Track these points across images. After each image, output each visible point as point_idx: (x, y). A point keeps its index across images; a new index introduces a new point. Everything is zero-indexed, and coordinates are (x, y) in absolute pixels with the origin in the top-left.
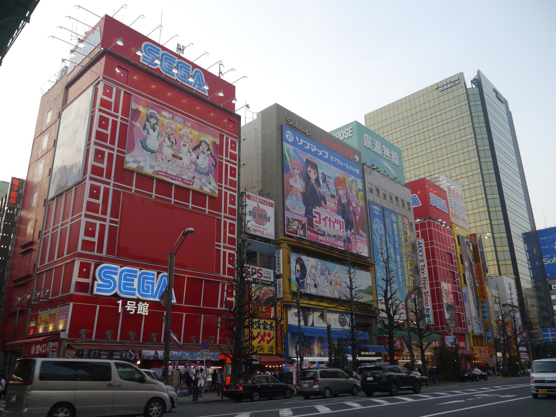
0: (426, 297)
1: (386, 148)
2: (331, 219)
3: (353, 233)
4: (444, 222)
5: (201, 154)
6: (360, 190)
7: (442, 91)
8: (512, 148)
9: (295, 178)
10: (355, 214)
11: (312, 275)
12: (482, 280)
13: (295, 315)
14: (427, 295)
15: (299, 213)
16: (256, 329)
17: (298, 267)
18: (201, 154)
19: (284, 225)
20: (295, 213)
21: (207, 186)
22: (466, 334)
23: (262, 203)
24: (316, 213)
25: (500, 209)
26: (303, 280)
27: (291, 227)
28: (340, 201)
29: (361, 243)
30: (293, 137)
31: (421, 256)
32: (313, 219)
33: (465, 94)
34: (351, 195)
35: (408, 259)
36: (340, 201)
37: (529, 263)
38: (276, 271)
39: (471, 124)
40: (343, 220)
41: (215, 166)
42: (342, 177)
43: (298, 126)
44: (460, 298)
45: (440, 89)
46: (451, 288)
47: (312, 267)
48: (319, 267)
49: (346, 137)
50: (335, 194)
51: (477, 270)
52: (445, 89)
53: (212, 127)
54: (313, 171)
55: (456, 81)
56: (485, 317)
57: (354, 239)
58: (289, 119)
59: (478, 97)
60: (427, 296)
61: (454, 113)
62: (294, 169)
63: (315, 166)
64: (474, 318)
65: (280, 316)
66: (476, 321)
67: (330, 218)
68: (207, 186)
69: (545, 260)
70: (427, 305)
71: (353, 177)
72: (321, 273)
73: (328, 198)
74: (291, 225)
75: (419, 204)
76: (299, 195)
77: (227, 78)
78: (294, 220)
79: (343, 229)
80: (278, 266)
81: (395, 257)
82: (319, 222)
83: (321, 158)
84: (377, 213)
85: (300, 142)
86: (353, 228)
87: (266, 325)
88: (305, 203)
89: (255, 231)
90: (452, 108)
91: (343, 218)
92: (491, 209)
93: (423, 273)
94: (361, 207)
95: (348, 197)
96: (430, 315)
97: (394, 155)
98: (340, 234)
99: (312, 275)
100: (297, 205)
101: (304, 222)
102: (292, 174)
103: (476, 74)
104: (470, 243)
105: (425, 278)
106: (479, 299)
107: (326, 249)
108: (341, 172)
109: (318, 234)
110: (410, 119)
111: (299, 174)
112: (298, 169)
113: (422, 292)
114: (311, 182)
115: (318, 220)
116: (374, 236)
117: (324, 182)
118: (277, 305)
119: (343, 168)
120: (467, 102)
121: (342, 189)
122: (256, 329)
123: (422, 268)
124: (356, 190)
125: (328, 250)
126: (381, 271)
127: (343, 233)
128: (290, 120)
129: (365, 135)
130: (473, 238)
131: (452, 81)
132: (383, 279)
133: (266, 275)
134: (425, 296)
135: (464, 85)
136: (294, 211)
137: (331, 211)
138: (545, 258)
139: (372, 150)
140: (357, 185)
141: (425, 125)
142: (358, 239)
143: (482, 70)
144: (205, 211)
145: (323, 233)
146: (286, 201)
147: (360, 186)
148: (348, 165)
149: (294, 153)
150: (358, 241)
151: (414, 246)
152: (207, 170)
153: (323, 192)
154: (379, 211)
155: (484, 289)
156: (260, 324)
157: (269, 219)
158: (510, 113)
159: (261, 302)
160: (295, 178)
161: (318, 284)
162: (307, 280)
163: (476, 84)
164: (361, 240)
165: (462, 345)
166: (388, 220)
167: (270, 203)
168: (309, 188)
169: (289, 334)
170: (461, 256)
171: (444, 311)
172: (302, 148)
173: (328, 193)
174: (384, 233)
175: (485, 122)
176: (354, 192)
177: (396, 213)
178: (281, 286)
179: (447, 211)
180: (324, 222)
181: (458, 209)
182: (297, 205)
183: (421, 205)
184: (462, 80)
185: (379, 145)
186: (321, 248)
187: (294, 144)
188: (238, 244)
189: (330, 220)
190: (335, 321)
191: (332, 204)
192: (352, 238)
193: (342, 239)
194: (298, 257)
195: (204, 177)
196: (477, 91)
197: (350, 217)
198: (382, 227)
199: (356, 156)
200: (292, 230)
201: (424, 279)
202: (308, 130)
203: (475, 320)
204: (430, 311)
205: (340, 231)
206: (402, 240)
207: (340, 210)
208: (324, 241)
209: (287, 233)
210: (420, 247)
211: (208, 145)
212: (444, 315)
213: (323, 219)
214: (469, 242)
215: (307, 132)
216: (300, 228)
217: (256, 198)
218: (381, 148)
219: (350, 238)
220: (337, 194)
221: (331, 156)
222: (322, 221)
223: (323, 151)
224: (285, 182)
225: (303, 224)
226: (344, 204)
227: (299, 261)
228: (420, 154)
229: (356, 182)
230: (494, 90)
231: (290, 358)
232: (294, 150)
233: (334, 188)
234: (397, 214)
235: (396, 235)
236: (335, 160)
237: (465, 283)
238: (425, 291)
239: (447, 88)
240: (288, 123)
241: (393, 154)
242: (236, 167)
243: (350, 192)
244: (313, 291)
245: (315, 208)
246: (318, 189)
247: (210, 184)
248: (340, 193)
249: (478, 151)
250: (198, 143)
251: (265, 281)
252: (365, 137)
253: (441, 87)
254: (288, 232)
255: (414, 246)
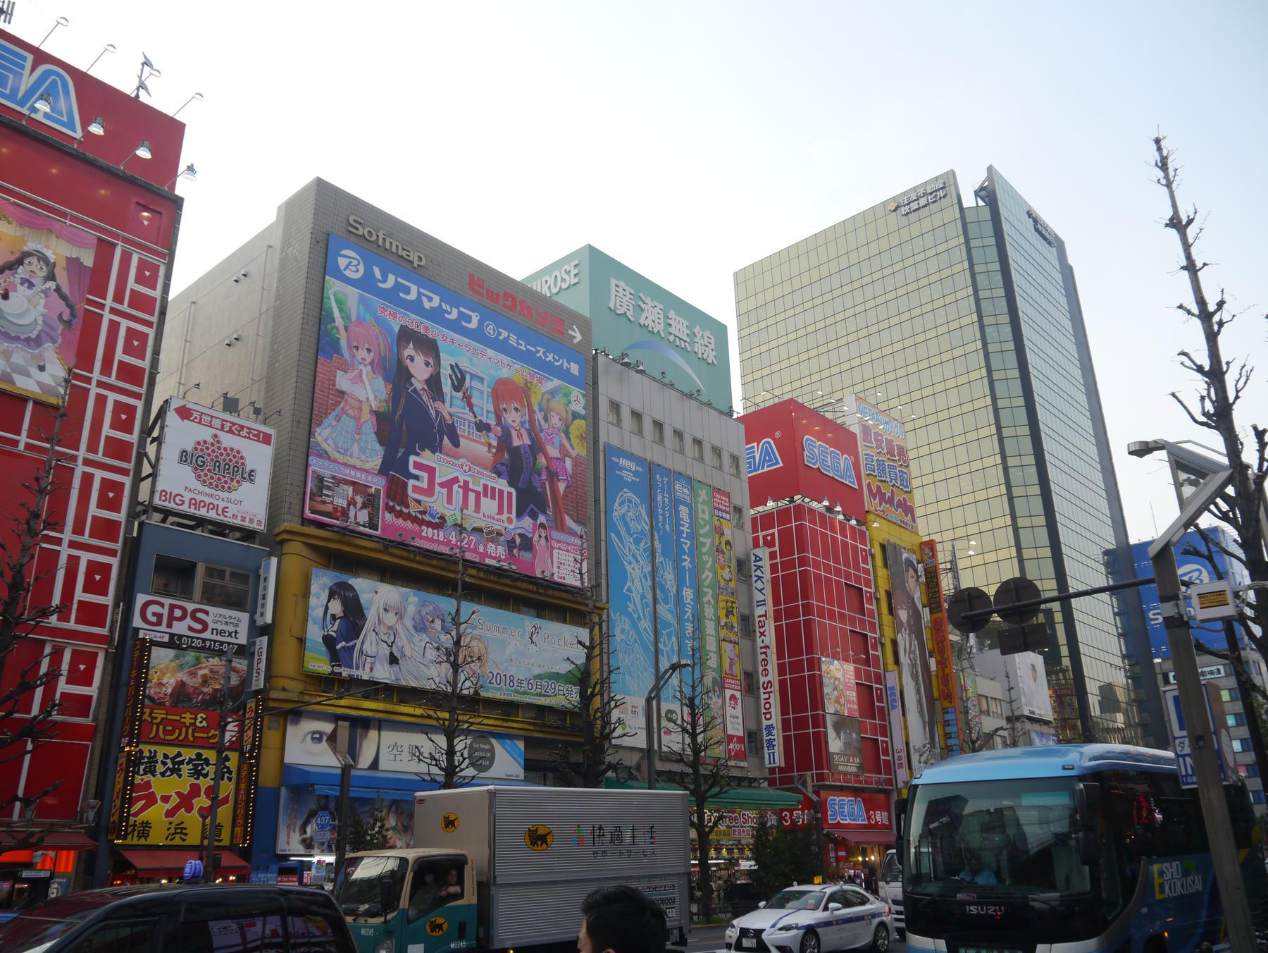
0: (767, 696)
1: (678, 318)
2: (471, 486)
3: (542, 526)
4: (838, 509)
5: (19, 287)
6: (576, 416)
7: (907, 214)
8: (1073, 348)
9: (356, 372)
10: (553, 476)
11: (382, 630)
12: (946, 656)
13: (313, 739)
14: (769, 690)
15: (358, 464)
16: (163, 774)
17: (336, 607)
18: (19, 287)
19: (304, 493)
20: (345, 464)
21: (28, 375)
22: (892, 790)
23: (230, 432)
24: (418, 466)
25: (1037, 490)
26: (351, 644)
27: (328, 500)
28: (505, 440)
29: (568, 551)
30: (361, 268)
31: (760, 591)
32: (407, 483)
33: (959, 222)
34: (545, 426)
35: (721, 597)
36: (505, 440)
37: (1119, 625)
38: (257, 617)
39: (970, 291)
40: (513, 491)
41: (68, 324)
42: (519, 380)
43: (384, 239)
44: (880, 700)
45: (903, 209)
46: (853, 673)
47: (385, 610)
48: (411, 609)
49: (565, 286)
50: (492, 422)
51: (934, 631)
52: (914, 211)
53: (73, 219)
54: (420, 359)
55: (939, 190)
56: (950, 748)
57: (543, 541)
58: (355, 221)
59: (988, 229)
60: (769, 693)
61: (933, 265)
62: (357, 348)
63: (429, 347)
64: (918, 750)
65: (250, 740)
66: (923, 759)
67: (466, 483)
68: (28, 375)
69: (1154, 614)
70: (768, 716)
71: (556, 382)
72: (415, 627)
73: (462, 430)
74: (328, 496)
75: (777, 463)
76: (366, 415)
77: (159, 99)
78: (338, 481)
79: (510, 511)
80: (263, 602)
81: (679, 592)
82: (430, 491)
83: (455, 326)
84: (629, 477)
85: (384, 280)
86: (544, 513)
87: (201, 765)
88: (381, 437)
89: (197, 505)
90: (929, 253)
91: (510, 484)
92: (1016, 492)
93: (762, 634)
94: (577, 462)
95: (533, 431)
96: (774, 743)
97: (702, 336)
98: (497, 526)
99: (382, 630)
100: (356, 444)
101: (373, 490)
102: (349, 361)
103: (984, 175)
104: (919, 563)
105: (767, 647)
106: (938, 704)
107: (435, 562)
108: (516, 366)
109: (422, 523)
110: (836, 282)
111: (372, 363)
112: (369, 350)
113: (758, 682)
114: (412, 385)
115: (424, 485)
116: (612, 535)
117: (457, 388)
118: (248, 710)
119: (526, 358)
120: (962, 239)
121: (516, 409)
122: (163, 774)
123: (760, 621)
124: (564, 414)
125: (443, 564)
126: (627, 627)
127: (506, 524)
128: (361, 224)
129: (613, 281)
130: (927, 550)
131: (929, 191)
132: (580, 642)
133: (220, 627)
134: (764, 693)
135: (955, 201)
136: (341, 459)
137: (472, 464)
138: (1152, 610)
139: (632, 319)
140: (570, 402)
141: (869, 295)
142: (559, 542)
143: (996, 166)
144: (16, 443)
145: (437, 520)
146: (318, 430)
147: (579, 406)
148: (542, 350)
149: (362, 308)
150: (556, 545)
151: (742, 566)
152: (36, 333)
153: (450, 414)
154: (636, 473)
155: (949, 678)
156: (182, 762)
157: (250, 475)
158: (1071, 269)
159: (190, 700)
160: (356, 372)
161: (404, 655)
162: (363, 644)
163: (986, 200)
164: (568, 544)
165: (878, 818)
166: (663, 497)
167: (259, 432)
168: (403, 401)
169: (283, 790)
170: (889, 594)
171: (826, 733)
172: (392, 296)
173: (470, 417)
174: (647, 528)
175: (1004, 287)
176: (555, 420)
177: (689, 480)
178: (264, 657)
179: (853, 483)
180: (445, 491)
181: (888, 480)
182: (356, 444)
183: (781, 465)
184: (953, 188)
185: (657, 310)
186: (417, 558)
187: (366, 284)
188: (126, 539)
189: (466, 487)
190: (395, 752)
191: (477, 446)
192: (536, 538)
193: (502, 539)
194: (338, 580)
195: (22, 349)
196: (986, 215)
197: (536, 484)
198: (644, 513)
199: (574, 330)
200: (329, 508)
201: (764, 650)
202: (417, 254)
203: (921, 755)
204: (774, 732)
205: (499, 517)
206: (704, 550)
207: (502, 464)
208: (438, 542)
209: (308, 513)
210: (759, 567)
211: (51, 266)
212: (827, 743)
213: (442, 485)
214: (915, 563)
215: (413, 257)
216: (359, 505)
217: (212, 417)
218: (661, 317)
219: (532, 539)
220: (499, 422)
221: (488, 325)
222: (437, 488)
223: (462, 309)
224: (321, 381)
225: (371, 495)
226: (518, 448)
227: (339, 591)
228: (856, 362)
229: (567, 395)
230: (1030, 214)
231: (285, 857)
232: (362, 301)
233: (491, 408)
234: (696, 485)
235: (685, 535)
236: (500, 334)
237: (897, 661)
238: (766, 679)
239: (919, 208)
240: (350, 229)
241: (699, 336)
242: (151, 332)
243: (542, 421)
244: (383, 674)
245: (418, 454)
246: (432, 406)
247: (42, 369)
248: (509, 421)
249: (987, 355)
250: (12, 258)
251: (215, 641)
252: (613, 288)
253: (904, 206)
254: (313, 512)
255: (742, 566)
